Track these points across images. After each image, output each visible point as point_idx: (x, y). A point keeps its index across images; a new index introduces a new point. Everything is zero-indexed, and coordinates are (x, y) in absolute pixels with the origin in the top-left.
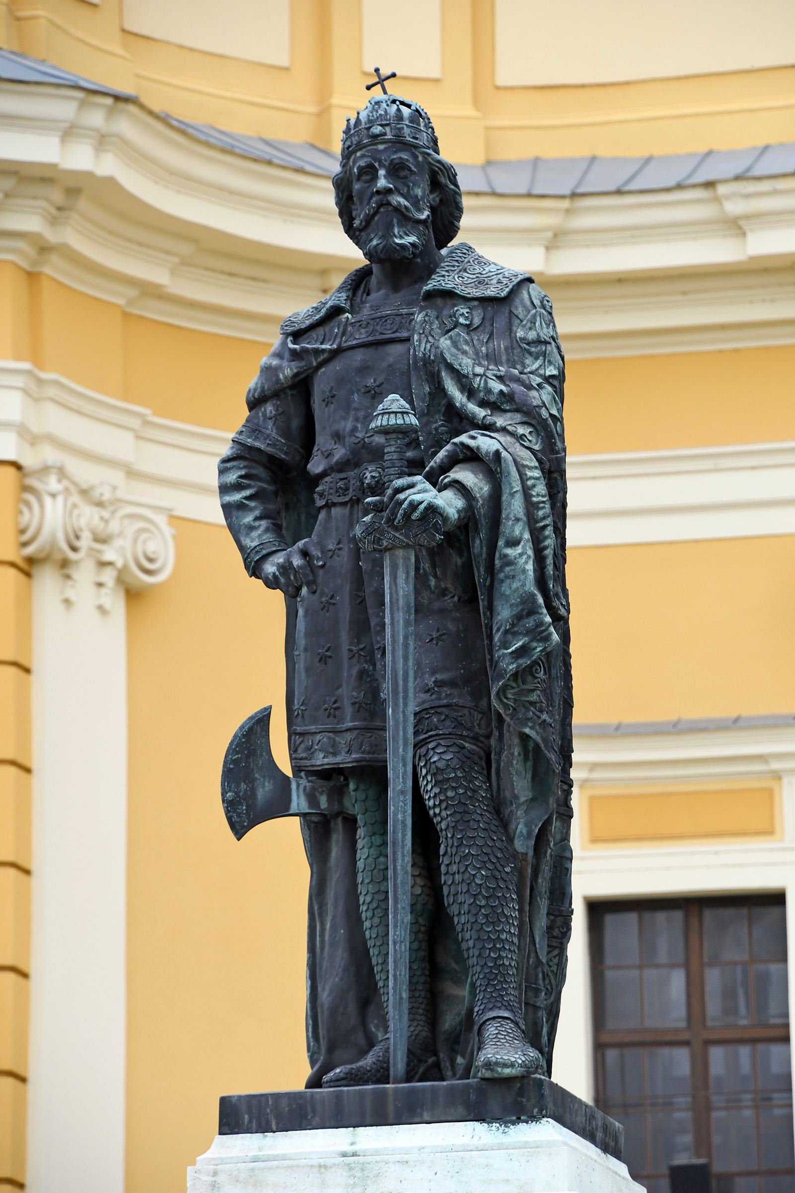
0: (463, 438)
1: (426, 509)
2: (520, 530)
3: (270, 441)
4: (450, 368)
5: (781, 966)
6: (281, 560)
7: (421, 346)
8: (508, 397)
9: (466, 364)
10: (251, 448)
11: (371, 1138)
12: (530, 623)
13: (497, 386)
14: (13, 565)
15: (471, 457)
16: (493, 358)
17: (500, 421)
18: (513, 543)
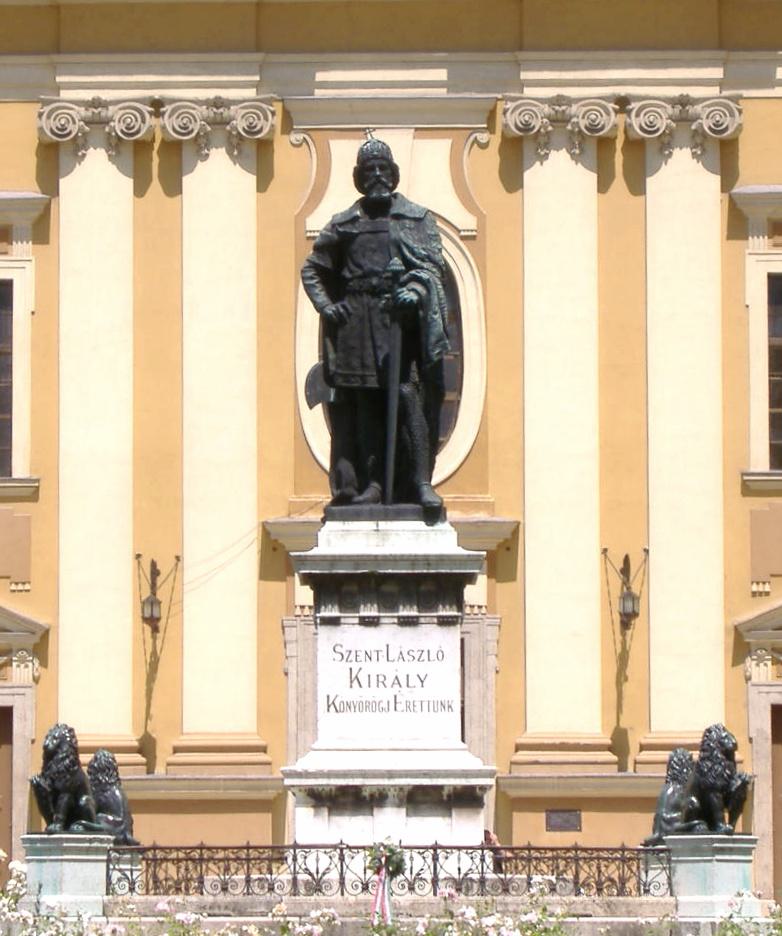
0: (413, 272)
3: (326, 262)
4: (405, 244)
5: (9, 746)
6: (334, 309)
9: (410, 243)
11: (383, 525)
12: (441, 343)
13: (424, 253)
16: (421, 241)
17: (425, 265)
18: (435, 313)
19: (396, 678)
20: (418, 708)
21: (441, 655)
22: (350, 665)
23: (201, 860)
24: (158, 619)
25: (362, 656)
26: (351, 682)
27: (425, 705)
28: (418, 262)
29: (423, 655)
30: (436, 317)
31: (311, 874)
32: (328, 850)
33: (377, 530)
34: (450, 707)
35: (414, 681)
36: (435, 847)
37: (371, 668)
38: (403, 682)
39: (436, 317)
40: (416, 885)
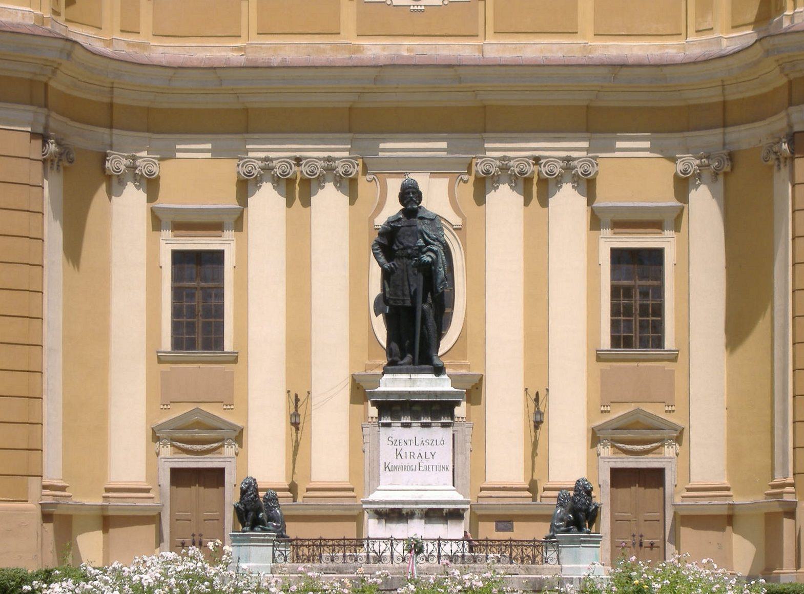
0: (429, 247)
1: (620, 346)
2: (441, 265)
4: (425, 232)
7: (419, 227)
8: (437, 239)
9: (428, 231)
10: (380, 243)
11: (413, 376)
12: (443, 283)
14: (41, 161)
15: (432, 251)
17: (435, 243)
18: (440, 268)
19: (420, 453)
20: (431, 469)
21: (668, 489)
22: (396, 447)
23: (321, 545)
24: (299, 424)
25: (402, 442)
26: (397, 456)
27: (434, 468)
28: (432, 241)
29: (433, 442)
30: (440, 270)
31: (376, 553)
32: (385, 541)
33: (410, 379)
34: (447, 468)
35: (429, 455)
36: (439, 540)
37: (407, 449)
38: (423, 456)
39: (440, 270)
40: (430, 559)
